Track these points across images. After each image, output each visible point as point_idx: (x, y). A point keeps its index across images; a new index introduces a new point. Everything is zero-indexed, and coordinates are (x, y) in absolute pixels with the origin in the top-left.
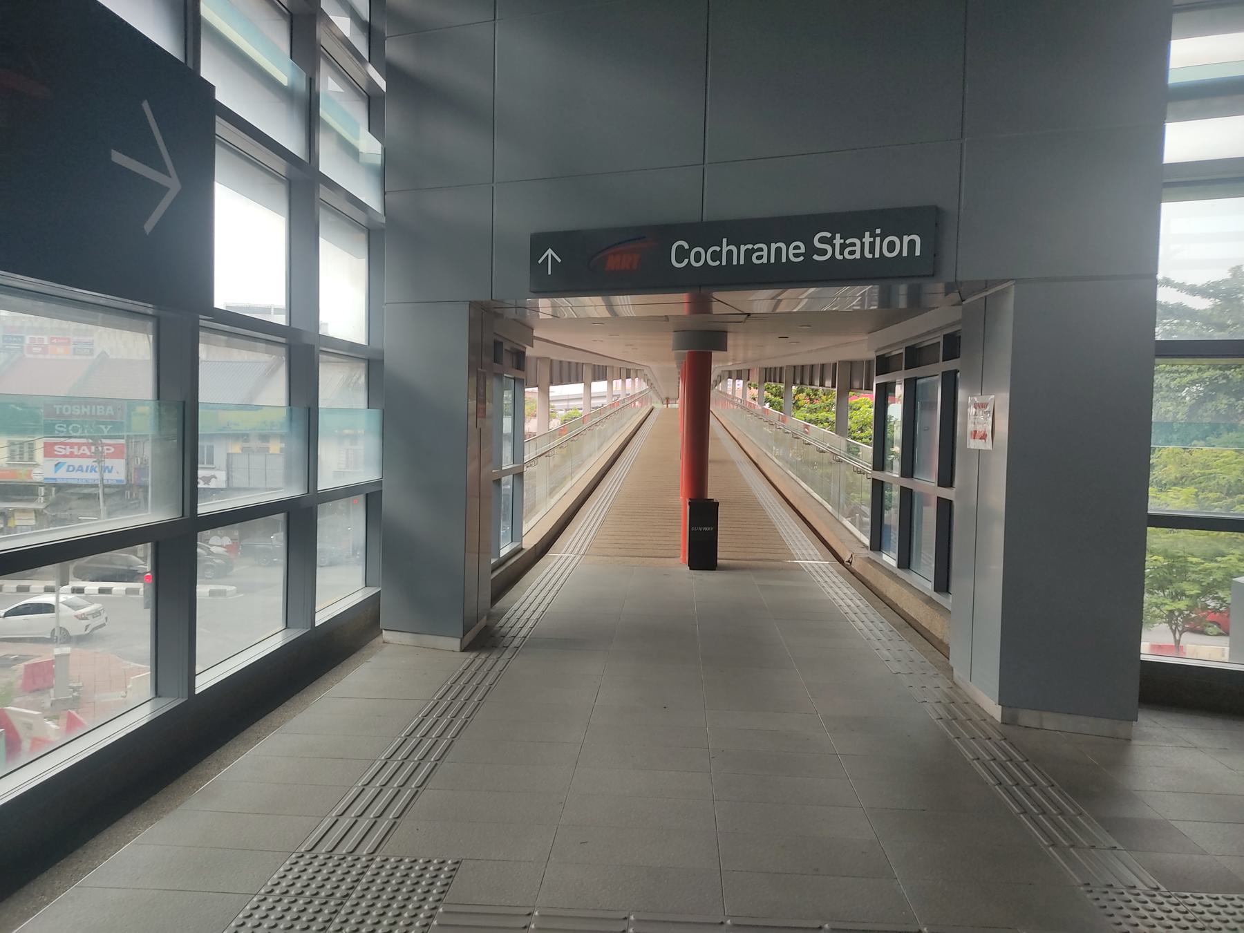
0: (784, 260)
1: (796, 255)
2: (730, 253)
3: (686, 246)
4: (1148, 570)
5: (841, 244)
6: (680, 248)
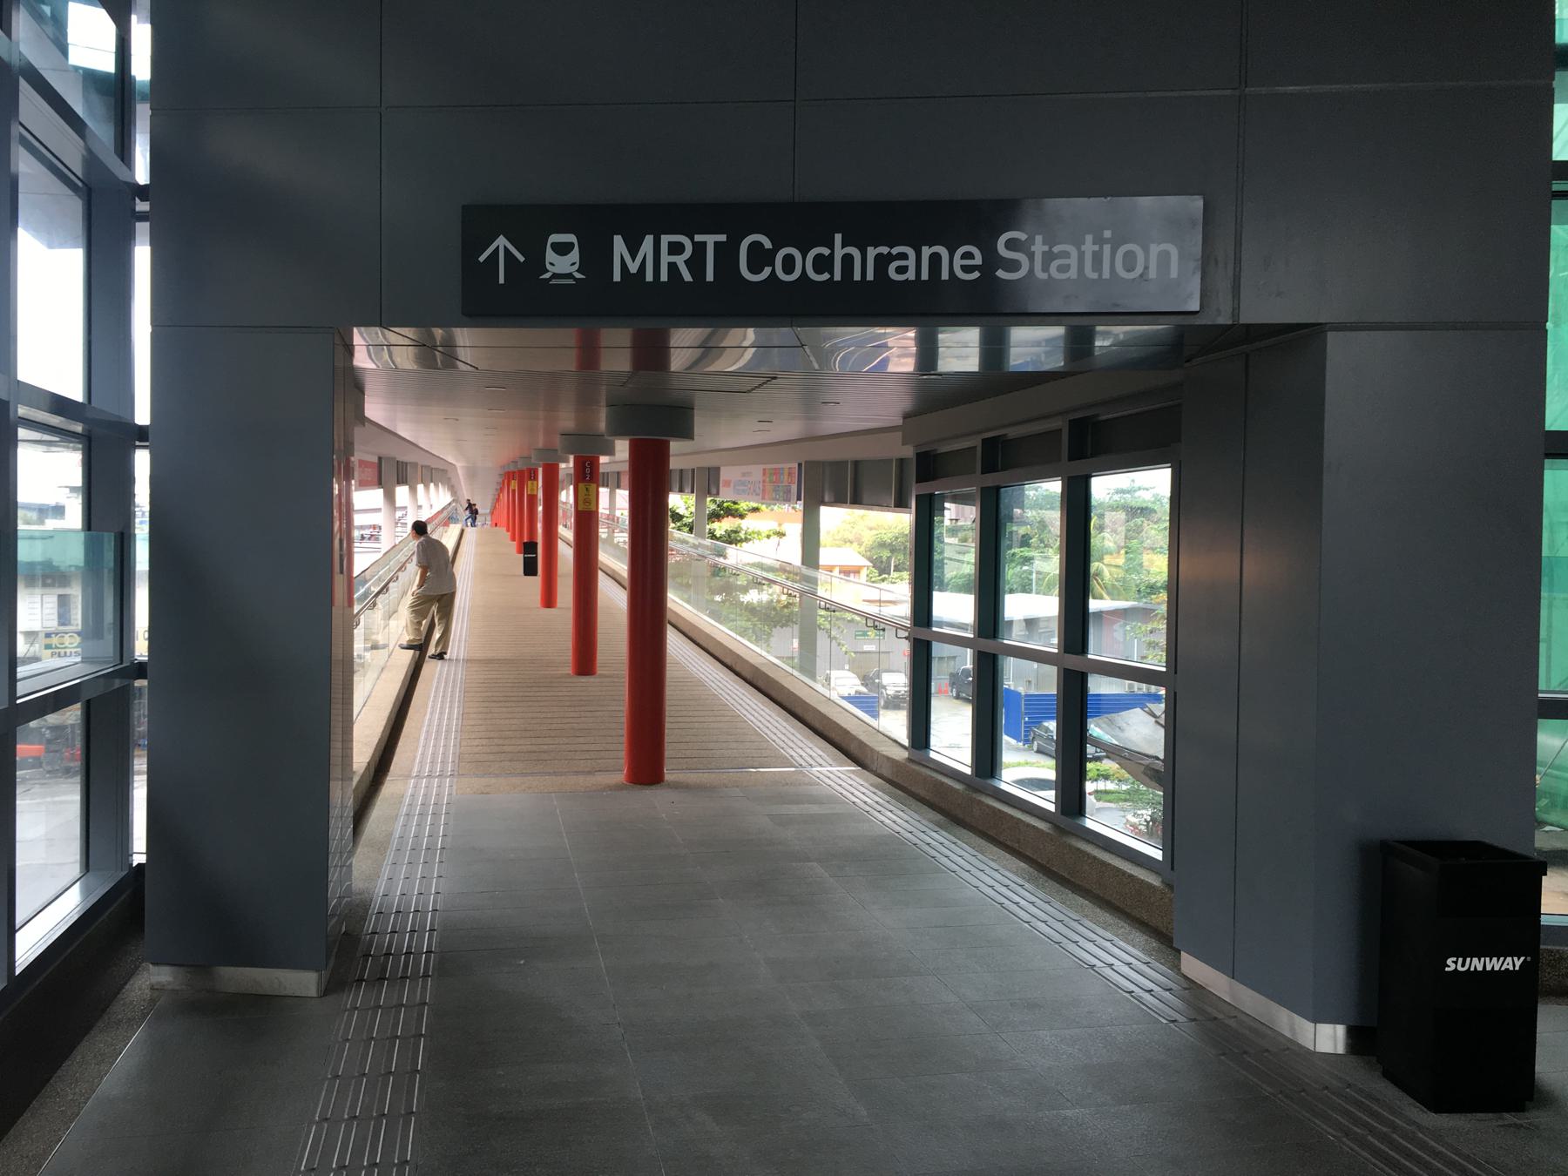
1: (966, 269)
3: (768, 244)
5: (1044, 253)
6: (755, 248)
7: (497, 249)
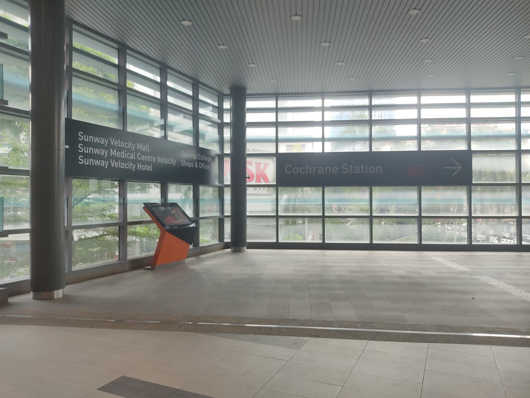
0: (93, 164)
1: (117, 166)
2: (309, 170)
4: (201, 241)
5: (352, 168)
6: (288, 167)
7: (458, 166)
